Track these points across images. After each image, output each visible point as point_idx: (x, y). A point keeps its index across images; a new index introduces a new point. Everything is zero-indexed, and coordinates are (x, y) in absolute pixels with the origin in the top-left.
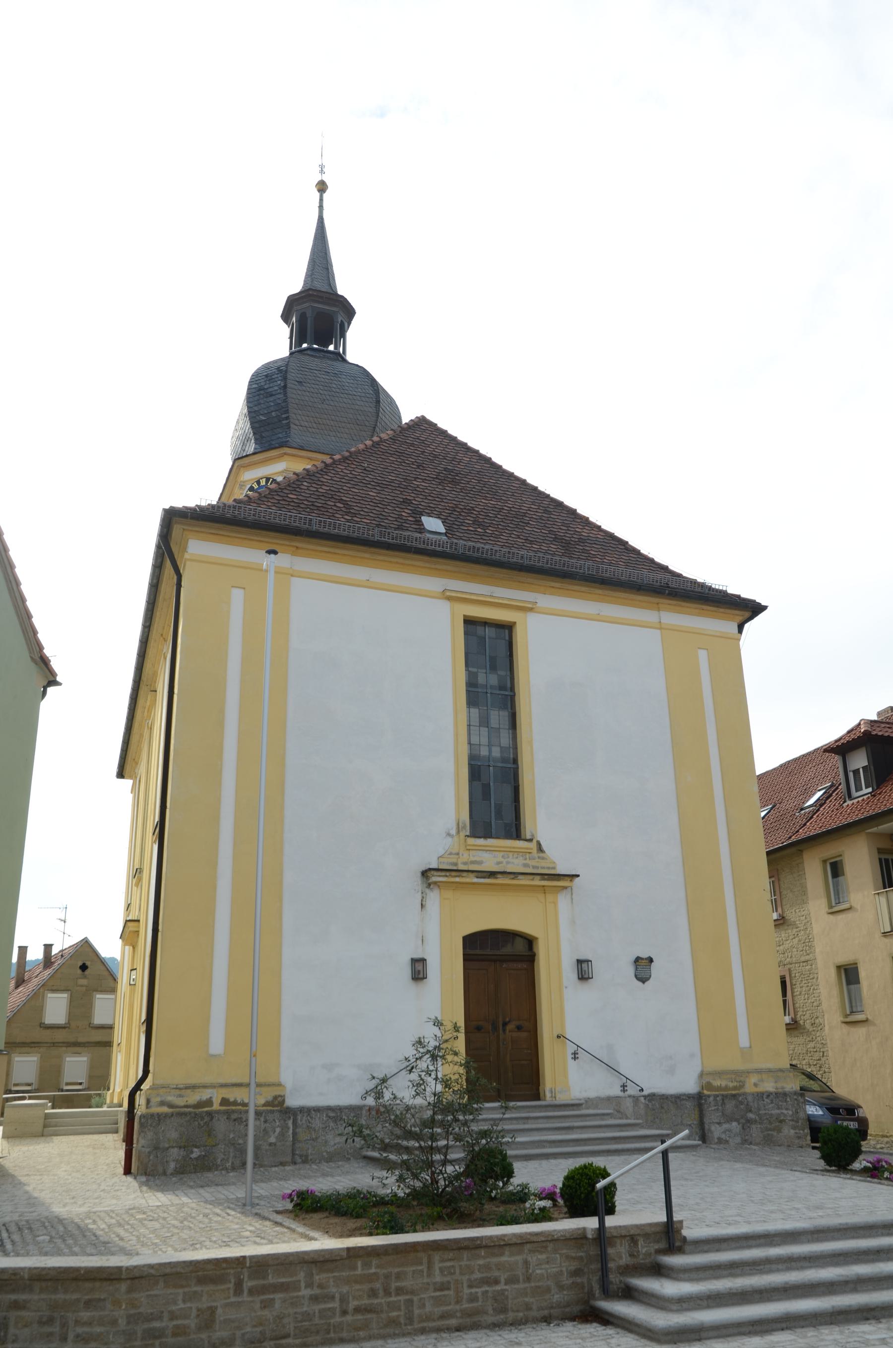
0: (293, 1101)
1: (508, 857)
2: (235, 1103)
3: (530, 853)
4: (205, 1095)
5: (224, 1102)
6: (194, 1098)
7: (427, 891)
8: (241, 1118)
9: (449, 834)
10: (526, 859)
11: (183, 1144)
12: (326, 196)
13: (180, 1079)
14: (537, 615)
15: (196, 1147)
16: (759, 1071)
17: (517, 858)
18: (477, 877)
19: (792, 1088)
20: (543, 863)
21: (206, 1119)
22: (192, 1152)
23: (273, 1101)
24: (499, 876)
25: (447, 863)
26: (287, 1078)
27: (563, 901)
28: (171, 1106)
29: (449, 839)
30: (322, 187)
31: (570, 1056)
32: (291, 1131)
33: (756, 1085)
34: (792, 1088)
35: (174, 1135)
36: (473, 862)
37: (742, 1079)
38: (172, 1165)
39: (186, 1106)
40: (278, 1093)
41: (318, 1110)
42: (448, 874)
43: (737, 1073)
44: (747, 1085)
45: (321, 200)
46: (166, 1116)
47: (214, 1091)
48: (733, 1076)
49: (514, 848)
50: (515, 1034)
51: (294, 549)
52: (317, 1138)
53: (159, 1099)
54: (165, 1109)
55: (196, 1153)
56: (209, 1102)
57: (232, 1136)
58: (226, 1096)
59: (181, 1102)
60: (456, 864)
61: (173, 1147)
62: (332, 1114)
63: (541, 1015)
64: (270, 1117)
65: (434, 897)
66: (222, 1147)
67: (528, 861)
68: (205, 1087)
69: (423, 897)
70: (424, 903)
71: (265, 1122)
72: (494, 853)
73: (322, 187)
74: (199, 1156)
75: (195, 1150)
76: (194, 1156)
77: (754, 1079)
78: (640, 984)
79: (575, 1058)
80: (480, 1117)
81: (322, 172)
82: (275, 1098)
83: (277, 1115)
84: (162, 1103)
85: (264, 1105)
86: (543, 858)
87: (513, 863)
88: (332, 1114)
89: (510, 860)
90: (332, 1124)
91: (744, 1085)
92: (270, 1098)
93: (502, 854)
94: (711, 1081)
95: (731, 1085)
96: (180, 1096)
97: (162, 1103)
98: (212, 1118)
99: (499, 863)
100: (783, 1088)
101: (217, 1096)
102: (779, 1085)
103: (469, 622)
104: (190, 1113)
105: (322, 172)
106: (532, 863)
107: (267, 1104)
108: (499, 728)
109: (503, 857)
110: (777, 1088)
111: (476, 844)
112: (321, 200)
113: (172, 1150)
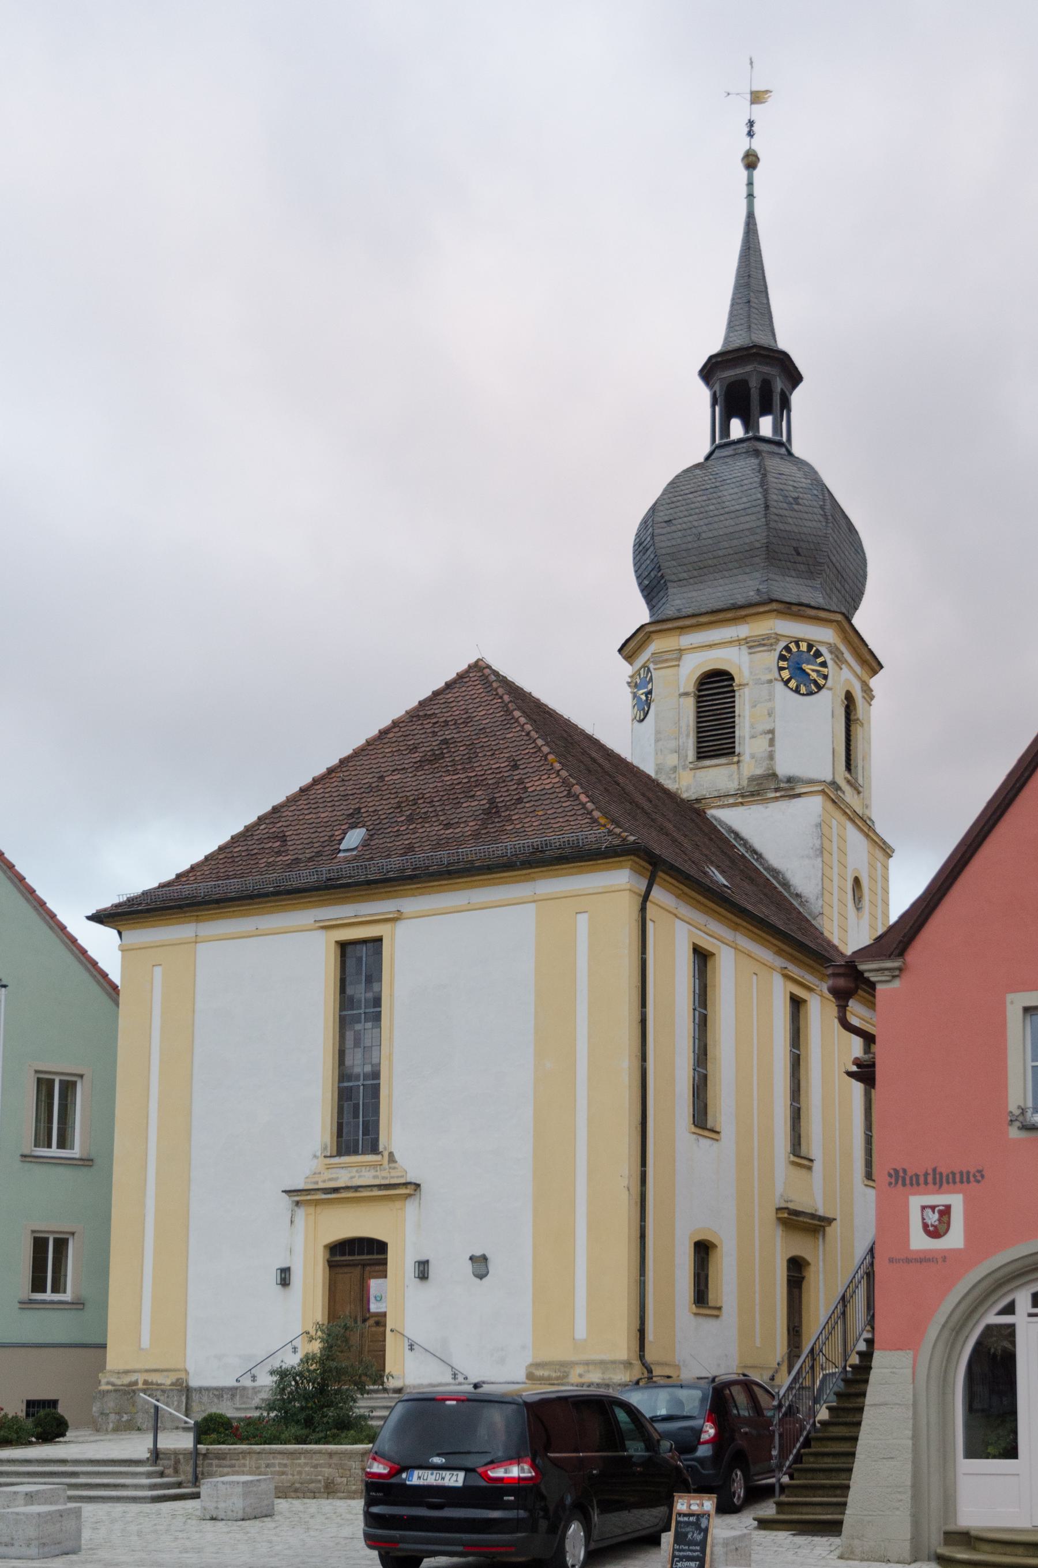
0: (194, 1382)
1: (361, 1171)
2: (152, 1383)
3: (381, 1165)
4: (133, 1378)
5: (146, 1382)
6: (126, 1380)
7: (296, 1208)
8: (153, 1394)
9: (315, 1156)
10: (377, 1171)
11: (117, 1411)
12: (757, 173)
13: (122, 1367)
14: (405, 921)
15: (126, 1414)
16: (587, 1363)
17: (369, 1171)
18: (325, 1194)
19: (621, 1379)
20: (394, 1173)
21: (132, 1394)
22: (123, 1417)
23: (176, 1382)
24: (342, 1191)
25: (311, 1183)
26: (191, 1367)
27: (410, 1208)
28: (113, 1385)
29: (316, 1161)
30: (751, 161)
31: (407, 1347)
32: (184, 1404)
33: (580, 1376)
34: (621, 1379)
35: (111, 1404)
36: (331, 1180)
37: (566, 1369)
38: (111, 1426)
39: (122, 1385)
40: (179, 1377)
41: (208, 1389)
42: (299, 1194)
43: (563, 1364)
44: (571, 1376)
45: (750, 184)
46: (108, 1391)
47: (139, 1374)
48: (558, 1367)
49: (364, 1162)
50: (374, 1329)
51: (195, 918)
52: (205, 1410)
53: (106, 1380)
54: (110, 1387)
55: (125, 1418)
56: (136, 1383)
57: (147, 1407)
58: (146, 1378)
59: (118, 1382)
60: (317, 1183)
61: (111, 1413)
62: (217, 1393)
63: (323, 1305)
64: (171, 1394)
65: (301, 1213)
66: (140, 1414)
67: (378, 1173)
68: (135, 1371)
69: (292, 1215)
70: (293, 1219)
71: (168, 1397)
72: (349, 1168)
73: (751, 161)
74: (127, 1420)
75: (125, 1415)
76: (124, 1419)
77: (579, 1370)
78: (478, 1280)
79: (411, 1349)
80: (357, 1405)
81: (751, 134)
82: (178, 1380)
83: (175, 1392)
84: (108, 1383)
85: (170, 1385)
86: (394, 1168)
87: (364, 1176)
88: (217, 1393)
89: (362, 1174)
90: (216, 1400)
91: (568, 1375)
92: (174, 1380)
93: (356, 1169)
94: (534, 1371)
95: (554, 1375)
96: (119, 1378)
97: (108, 1383)
98: (135, 1394)
99: (352, 1178)
100: (610, 1379)
101: (141, 1378)
102: (607, 1376)
103: (344, 947)
104: (122, 1390)
105: (751, 134)
106: (384, 1174)
107: (172, 1384)
108: (372, 1046)
109: (357, 1171)
110: (603, 1379)
111: (331, 1162)
112: (750, 184)
113: (111, 1415)
